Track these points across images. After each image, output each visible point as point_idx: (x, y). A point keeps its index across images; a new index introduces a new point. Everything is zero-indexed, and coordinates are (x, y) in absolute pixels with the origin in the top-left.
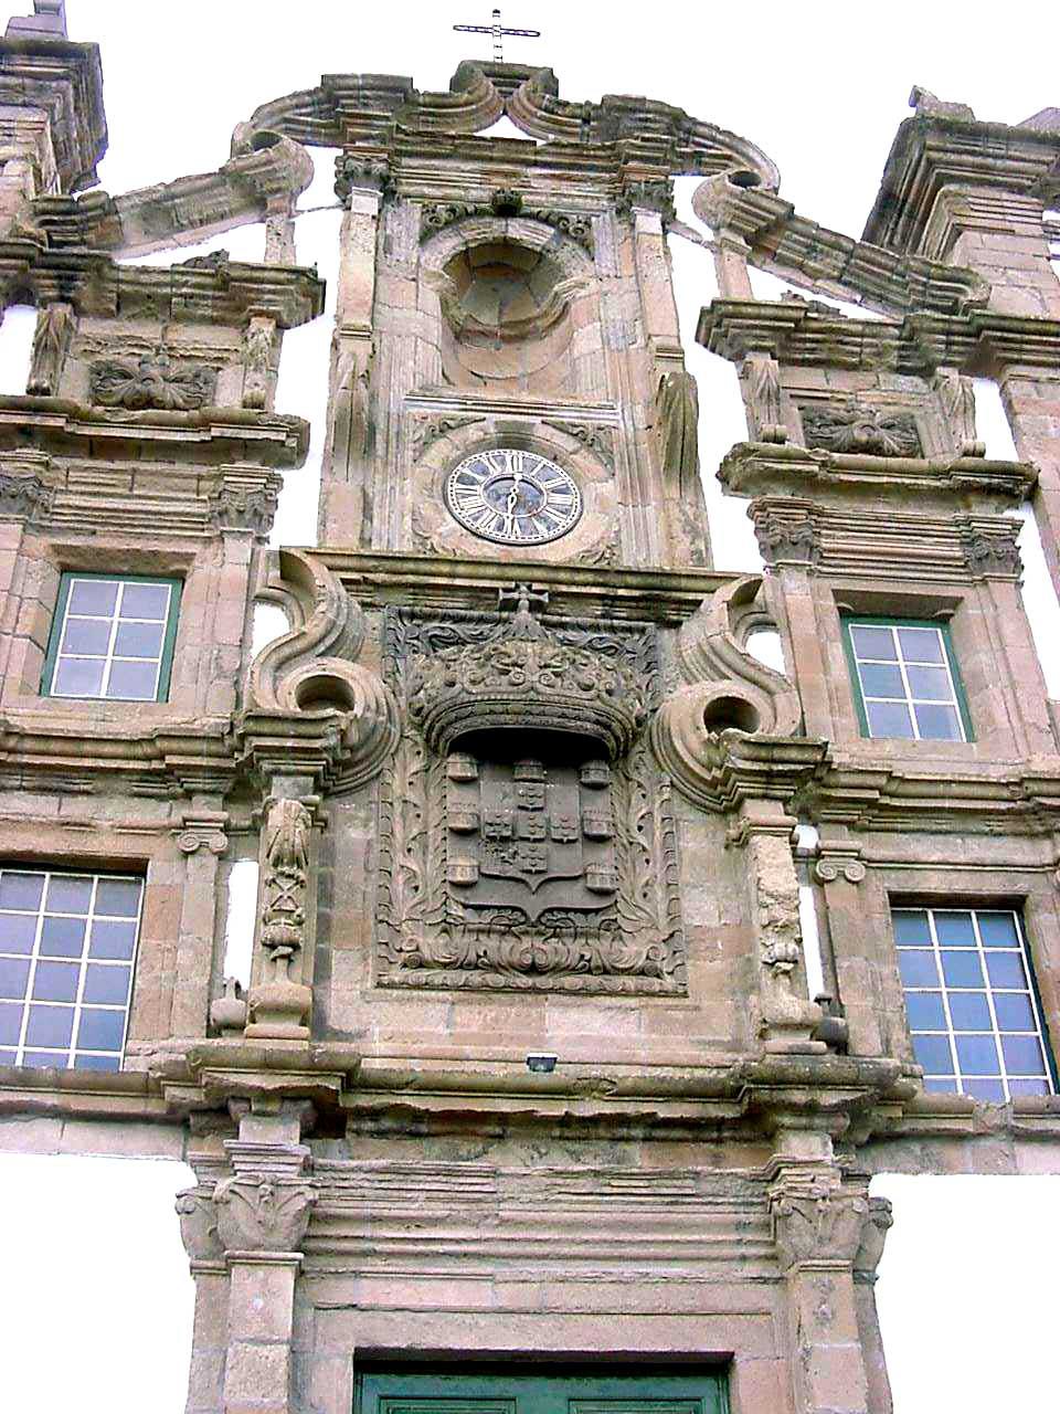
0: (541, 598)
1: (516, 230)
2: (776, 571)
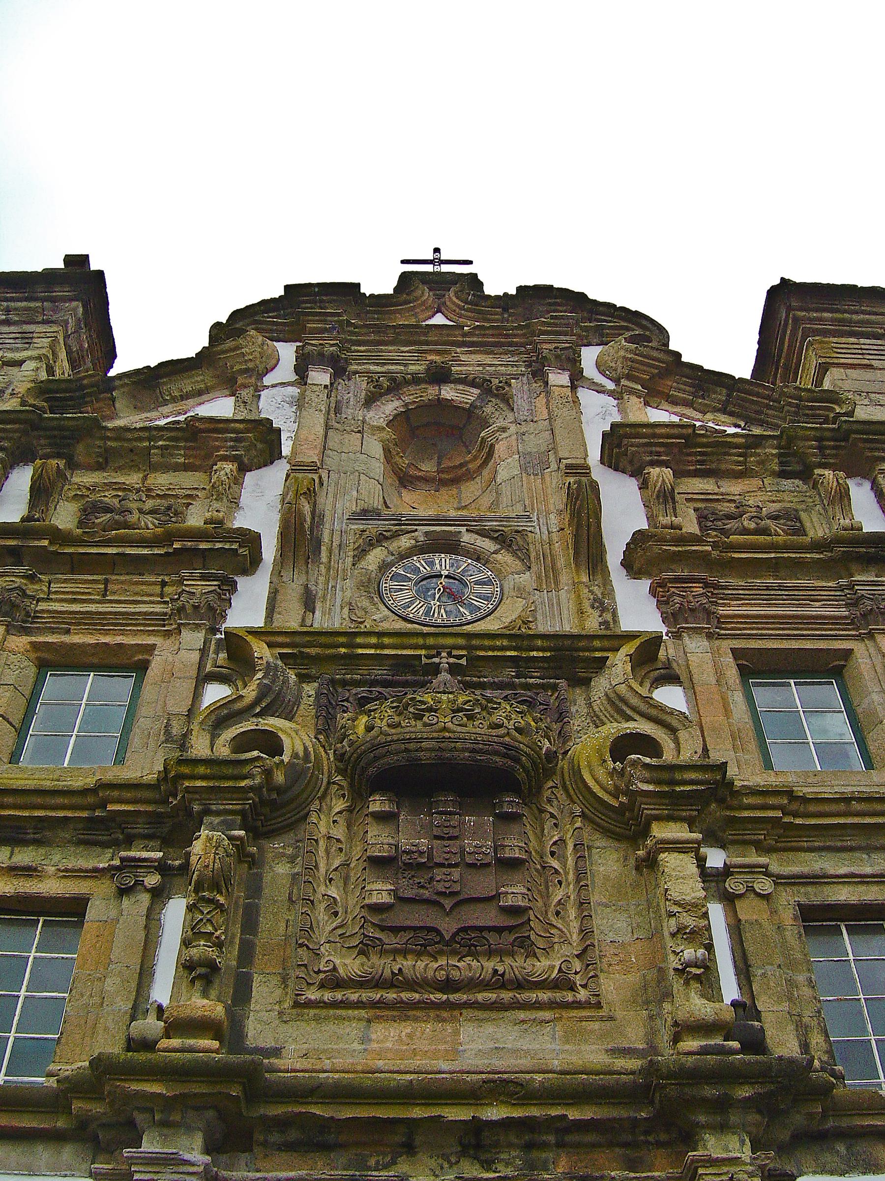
0: (459, 661)
1: (448, 392)
2: (677, 635)
